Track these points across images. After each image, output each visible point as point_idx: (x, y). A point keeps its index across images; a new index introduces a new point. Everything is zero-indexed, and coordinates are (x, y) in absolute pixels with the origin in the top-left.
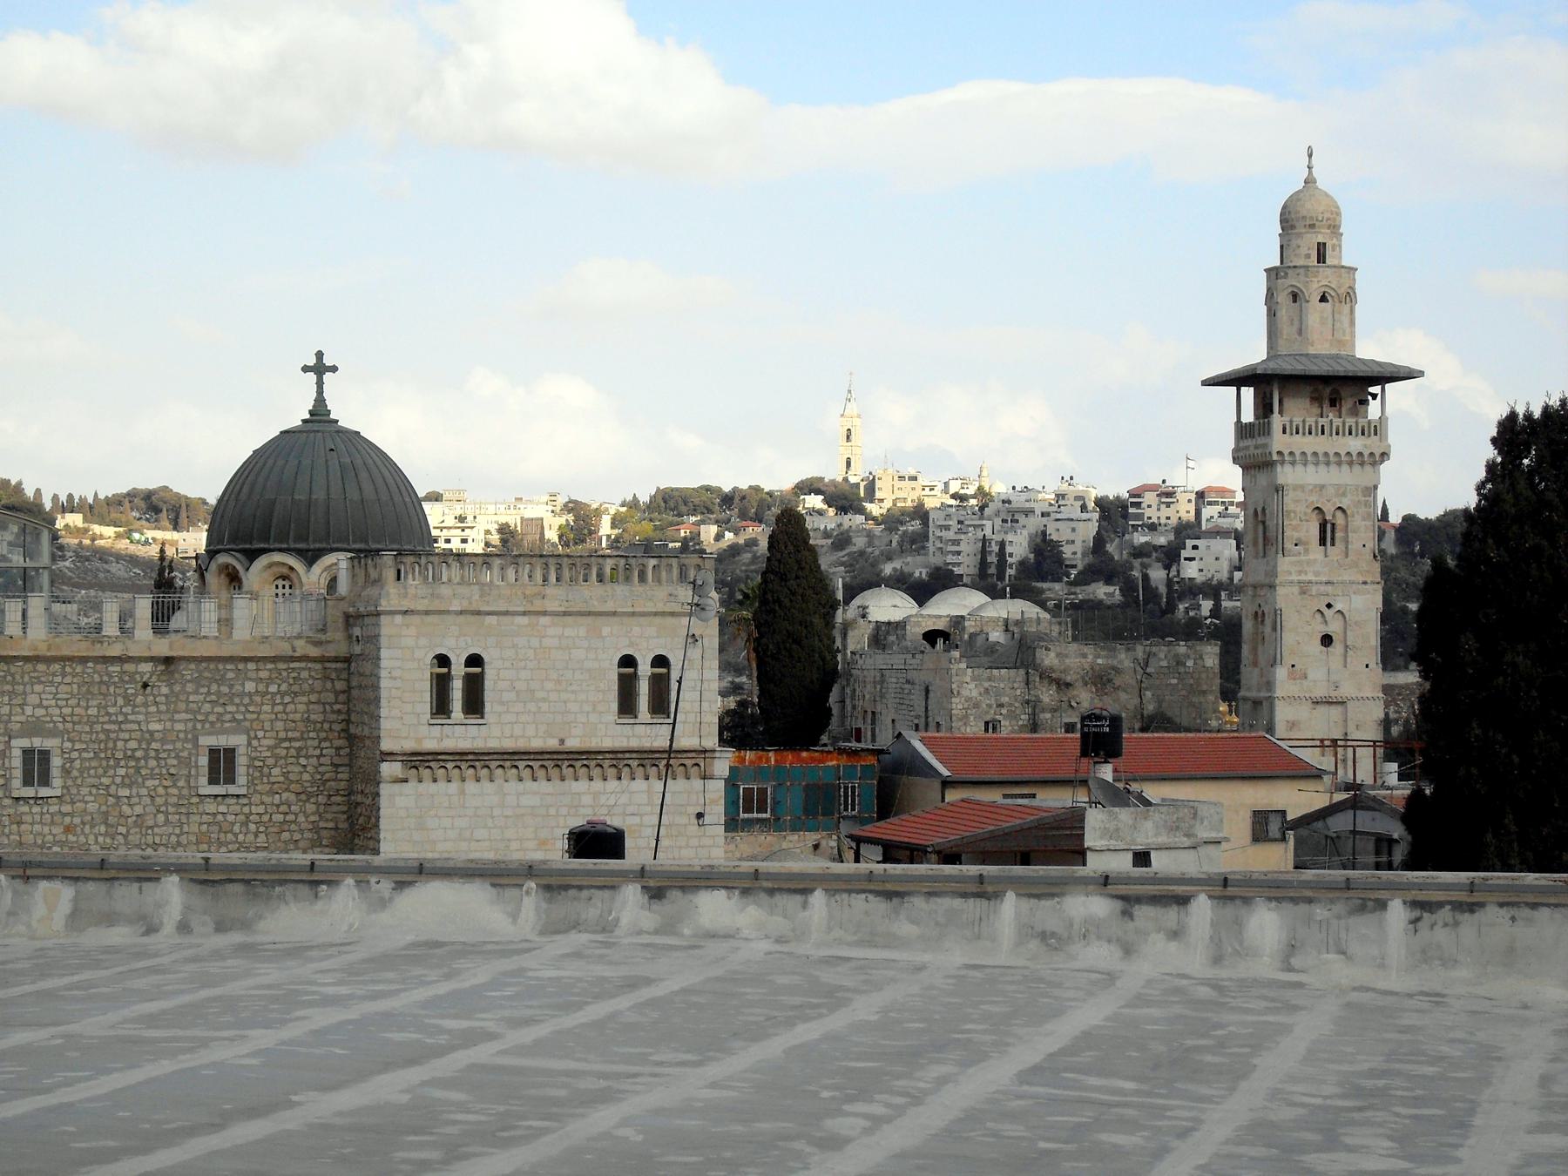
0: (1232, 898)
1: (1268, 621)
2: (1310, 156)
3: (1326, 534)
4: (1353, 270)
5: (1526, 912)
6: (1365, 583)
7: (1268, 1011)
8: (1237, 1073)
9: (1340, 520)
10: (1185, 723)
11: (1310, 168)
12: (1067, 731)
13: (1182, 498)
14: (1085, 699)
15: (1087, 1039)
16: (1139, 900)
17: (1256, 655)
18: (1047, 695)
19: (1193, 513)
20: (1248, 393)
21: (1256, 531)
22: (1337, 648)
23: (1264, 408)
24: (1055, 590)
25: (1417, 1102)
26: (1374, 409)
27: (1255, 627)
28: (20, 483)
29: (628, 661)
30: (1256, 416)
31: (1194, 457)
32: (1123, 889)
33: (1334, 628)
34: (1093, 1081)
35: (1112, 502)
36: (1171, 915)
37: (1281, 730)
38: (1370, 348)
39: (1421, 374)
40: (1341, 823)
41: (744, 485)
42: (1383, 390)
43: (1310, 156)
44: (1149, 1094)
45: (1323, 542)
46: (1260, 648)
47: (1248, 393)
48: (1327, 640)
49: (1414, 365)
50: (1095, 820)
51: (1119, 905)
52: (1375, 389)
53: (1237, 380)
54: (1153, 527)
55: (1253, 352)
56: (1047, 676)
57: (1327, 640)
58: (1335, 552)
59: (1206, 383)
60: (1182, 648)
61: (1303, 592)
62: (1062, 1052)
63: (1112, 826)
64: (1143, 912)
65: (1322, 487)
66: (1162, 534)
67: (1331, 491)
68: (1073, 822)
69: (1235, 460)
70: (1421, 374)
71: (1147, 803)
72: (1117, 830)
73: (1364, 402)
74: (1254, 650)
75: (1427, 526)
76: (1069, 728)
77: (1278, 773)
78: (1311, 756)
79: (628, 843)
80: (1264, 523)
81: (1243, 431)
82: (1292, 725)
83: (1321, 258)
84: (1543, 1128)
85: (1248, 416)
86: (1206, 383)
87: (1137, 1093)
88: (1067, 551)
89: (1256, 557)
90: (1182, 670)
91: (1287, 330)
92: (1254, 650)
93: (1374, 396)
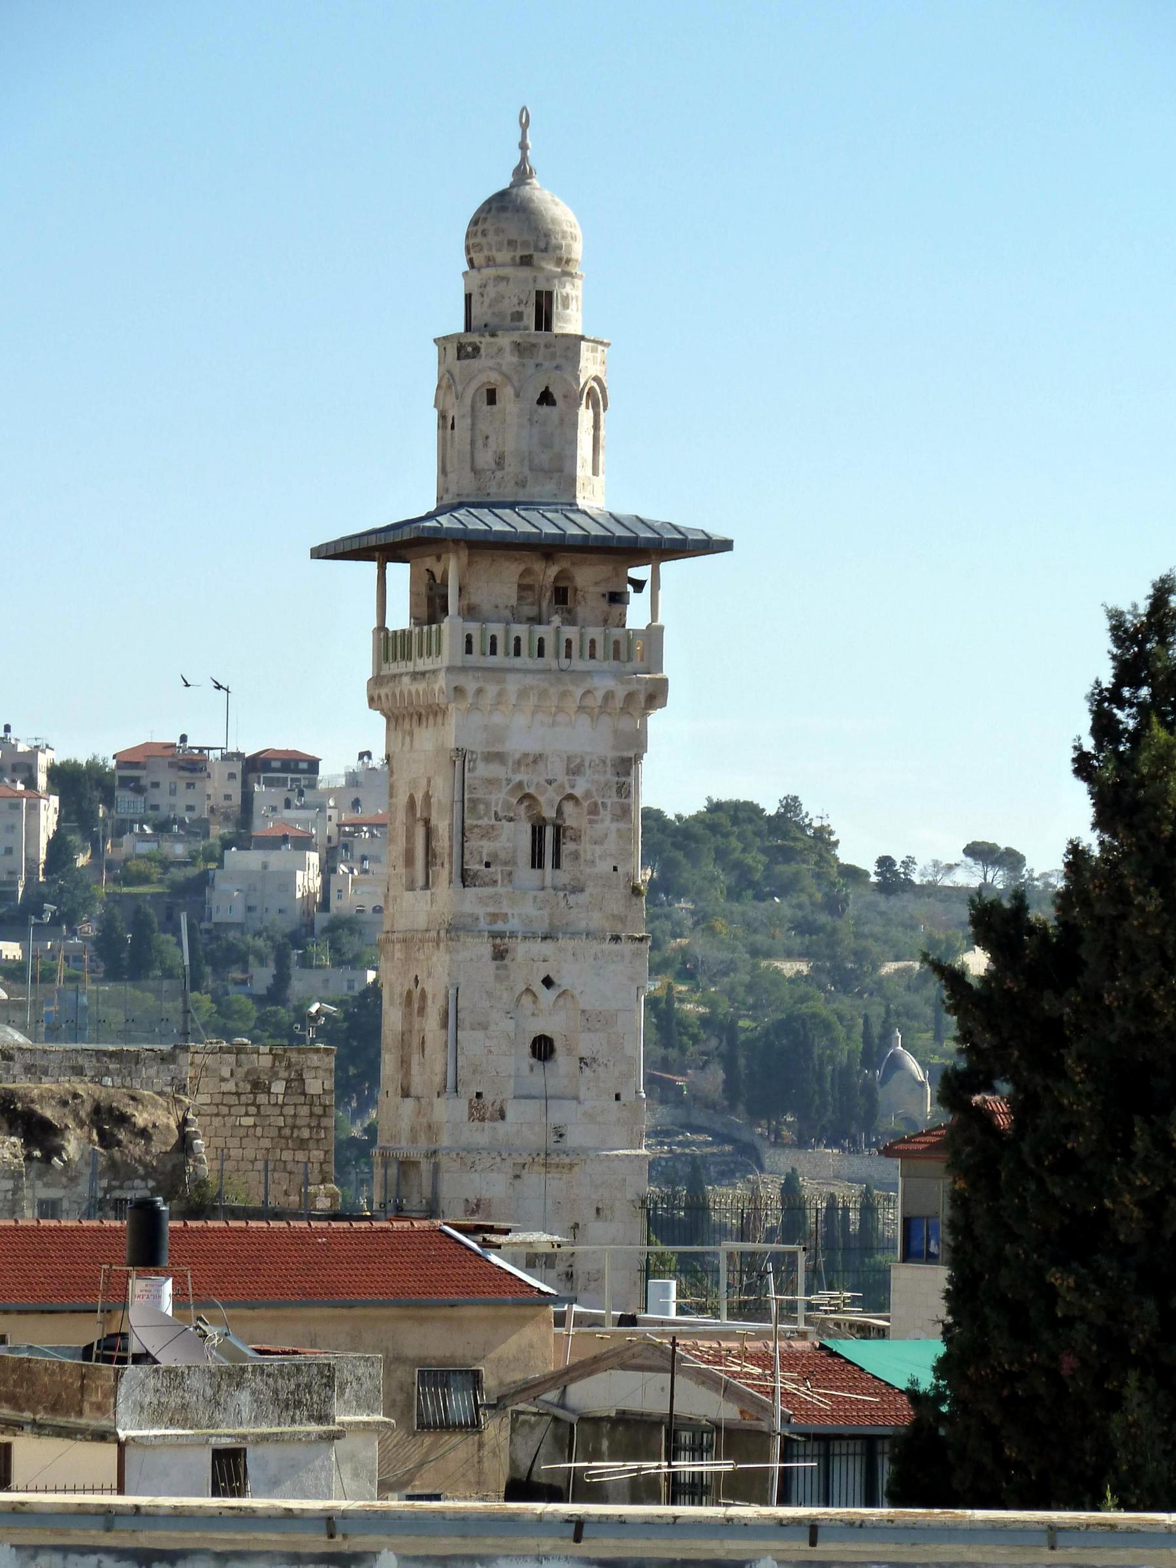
2: (524, 126)
6: (616, 939)
11: (523, 147)
12: (43, 1215)
13: (219, 773)
17: (407, 1074)
19: (237, 799)
21: (410, 837)
23: (431, 604)
26: (637, 613)
27: (407, 1017)
28: (791, 804)
30: (416, 619)
38: (607, 491)
41: (83, 759)
42: (655, 574)
43: (524, 126)
45: (537, 861)
46: (415, 1059)
47: (399, 574)
48: (543, 1048)
49: (718, 532)
52: (640, 572)
55: (409, 491)
57: (543, 1048)
61: (500, 955)
63: (174, 1401)
65: (538, 759)
66: (178, 838)
67: (556, 769)
69: (373, 702)
72: (184, 1407)
73: (617, 599)
74: (404, 1063)
77: (56, 1303)
80: (427, 822)
81: (390, 646)
85: (399, 618)
89: (411, 887)
90: (262, 1099)
92: (404, 1063)
93: (639, 585)
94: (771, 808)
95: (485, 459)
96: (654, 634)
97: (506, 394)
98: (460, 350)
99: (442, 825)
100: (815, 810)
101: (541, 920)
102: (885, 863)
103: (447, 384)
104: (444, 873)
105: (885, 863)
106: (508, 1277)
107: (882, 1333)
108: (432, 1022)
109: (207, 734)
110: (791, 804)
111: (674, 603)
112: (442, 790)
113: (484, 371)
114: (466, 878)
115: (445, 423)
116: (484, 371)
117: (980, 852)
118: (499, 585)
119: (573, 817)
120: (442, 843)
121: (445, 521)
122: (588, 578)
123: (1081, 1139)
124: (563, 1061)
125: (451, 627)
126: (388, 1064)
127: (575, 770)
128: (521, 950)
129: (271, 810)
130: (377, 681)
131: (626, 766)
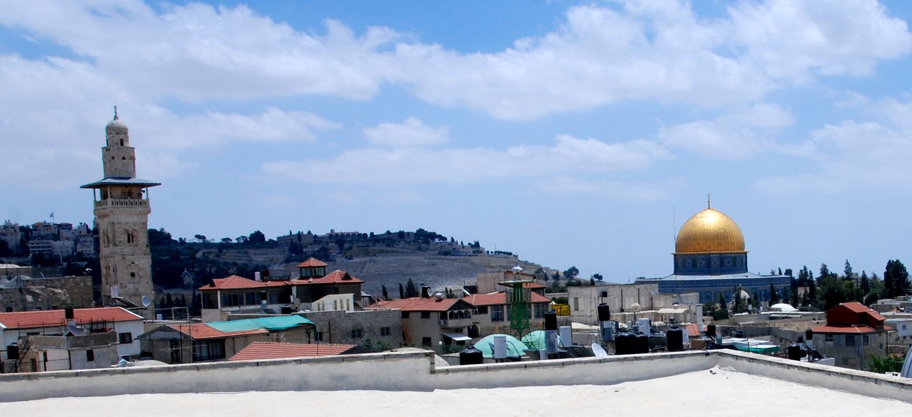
0: (217, 349)
1: (111, 269)
3: (130, 238)
4: (133, 149)
20: (98, 191)
23: (104, 196)
26: (144, 197)
29: (335, 302)
31: (80, 211)
35: (193, 247)
38: (140, 176)
45: (129, 241)
47: (98, 191)
48: (133, 275)
52: (144, 189)
53: (94, 186)
55: (99, 176)
57: (133, 275)
59: (82, 187)
60: (78, 278)
61: (123, 258)
73: (141, 195)
74: (107, 279)
79: (384, 326)
81: (97, 204)
83: (122, 144)
85: (99, 199)
86: (82, 187)
92: (107, 279)
94: (159, 230)
95: (113, 169)
96: (148, 199)
97: (116, 158)
98: (106, 150)
99: (110, 236)
100: (167, 231)
101: (131, 252)
102: (181, 239)
103: (104, 156)
104: (111, 245)
105: (181, 239)
106: (80, 305)
107: (200, 322)
108: (111, 271)
109: (49, 221)
110: (162, 229)
111: (150, 194)
112: (110, 230)
113: (112, 153)
114: (115, 245)
115: (105, 163)
116: (112, 153)
117: (198, 237)
118: (118, 192)
119: (135, 234)
120: (111, 239)
121: (106, 181)
122: (134, 190)
123: (596, 334)
124: (137, 277)
125: (109, 200)
126: (103, 279)
127: (135, 225)
128: (128, 258)
129: (65, 233)
130: (95, 210)
131: (145, 224)
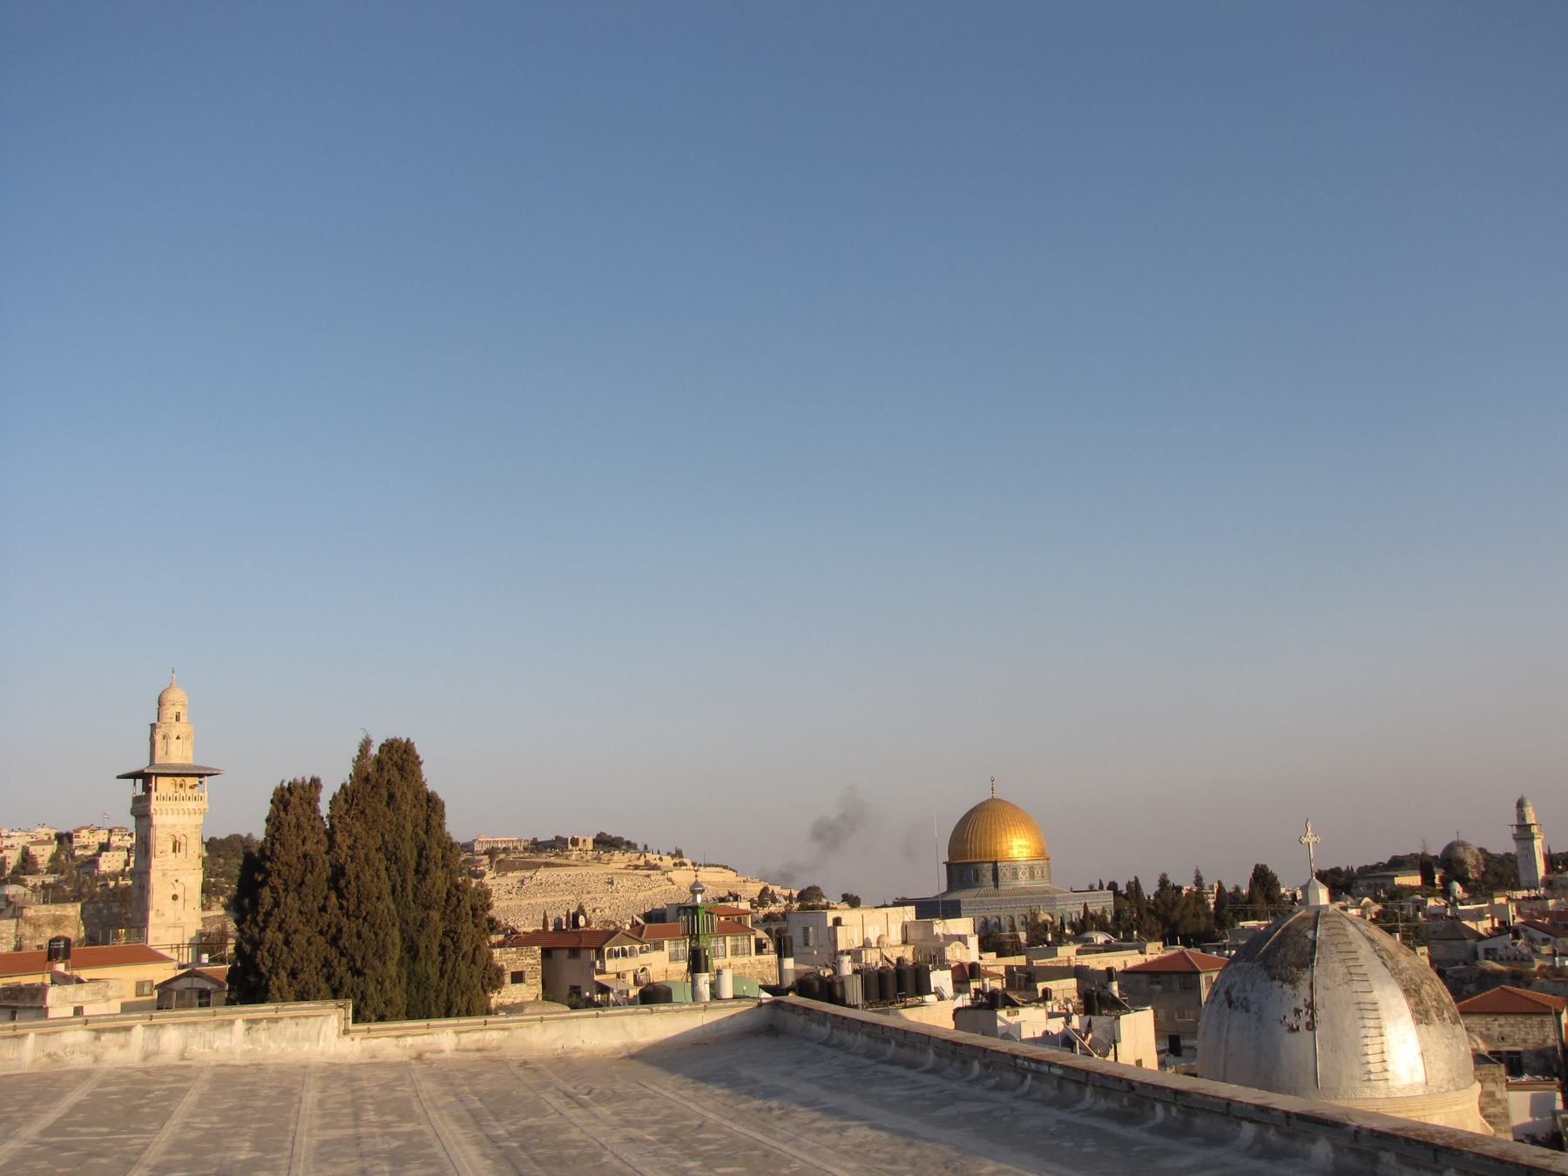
3: (176, 847)
5: (303, 1020)
7: (174, 1082)
8: (164, 1117)
9: (183, 840)
10: (1144, 978)
14: (50, 933)
15: (77, 1107)
16: (104, 1030)
18: (28, 931)
20: (139, 782)
22: (180, 900)
24: (31, 880)
25: (261, 1120)
32: (95, 1026)
33: (179, 891)
34: (84, 1130)
36: (122, 1036)
37: (151, 942)
39: (1198, 872)
40: (186, 983)
44: (117, 1133)
47: (139, 782)
48: (175, 897)
50: (53, 994)
51: (93, 1034)
53: (134, 776)
54: (85, 847)
56: (28, 921)
58: (181, 855)
62: (66, 1116)
64: (105, 1037)
68: (38, 992)
70: (1198, 872)
71: (80, 981)
75: (222, 842)
76: (40, 947)
78: (166, 952)
82: (156, 939)
84: (324, 1127)
87: (110, 1133)
88: (40, 860)
91: (159, 752)
